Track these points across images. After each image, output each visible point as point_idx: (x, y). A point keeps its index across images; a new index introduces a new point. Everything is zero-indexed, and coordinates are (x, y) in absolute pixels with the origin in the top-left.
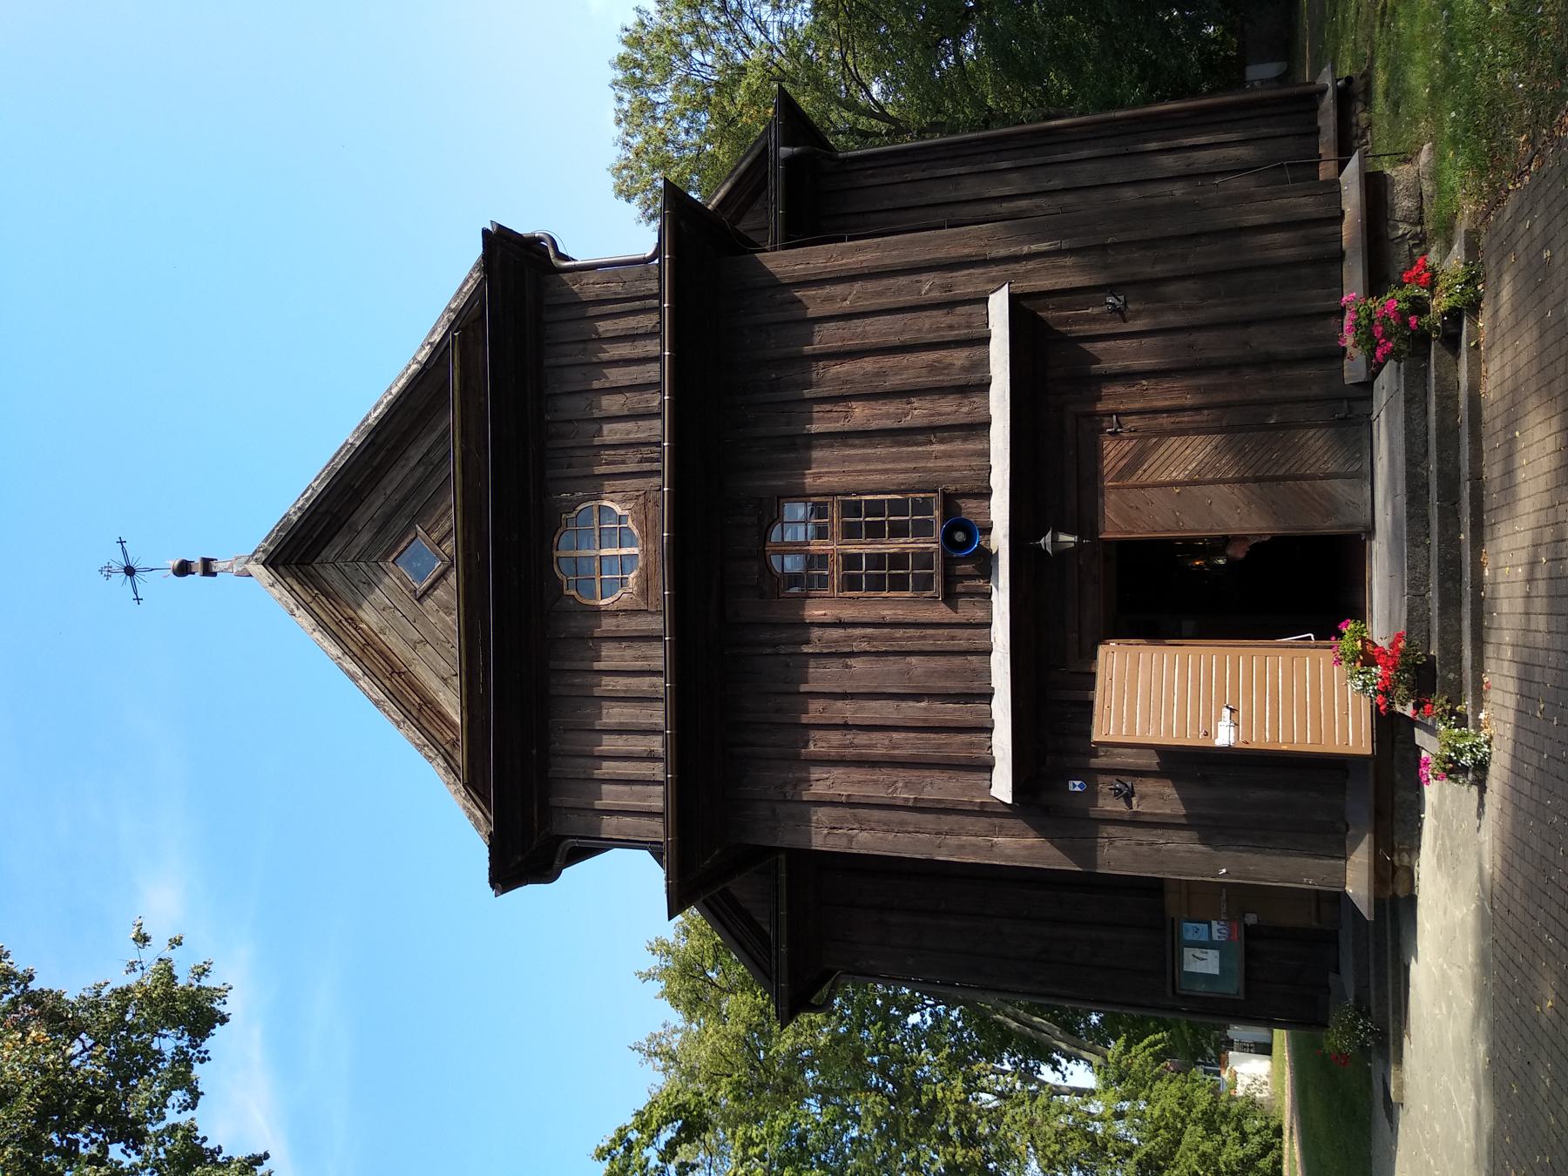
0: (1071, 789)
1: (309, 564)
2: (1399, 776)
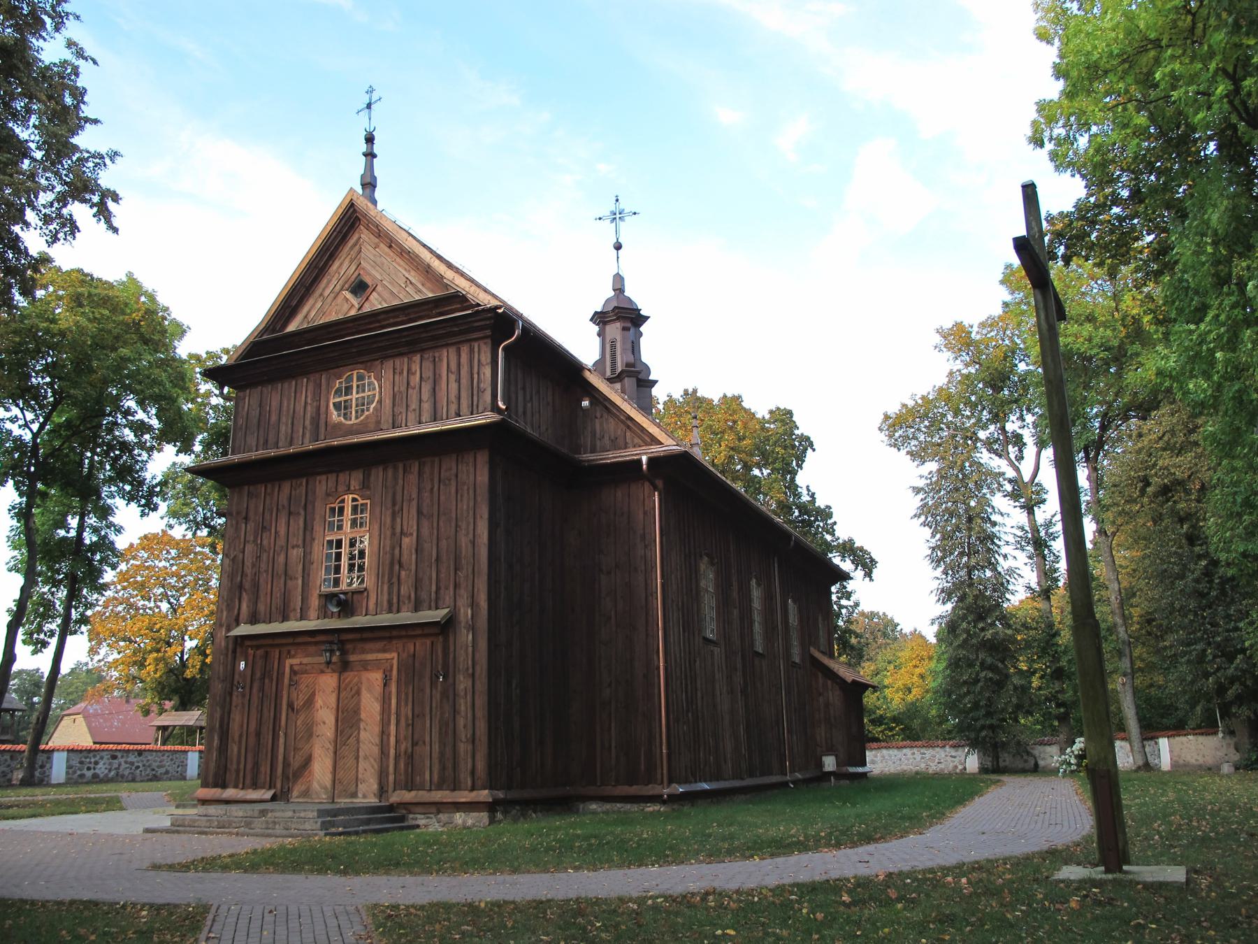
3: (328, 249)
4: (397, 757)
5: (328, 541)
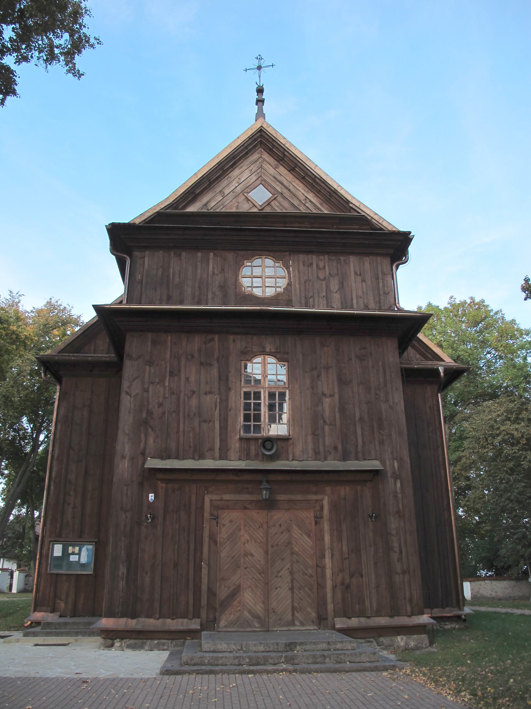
0: (150, 495)
1: (261, 146)
2: (156, 642)
3: (234, 158)
4: (334, 587)
5: (245, 393)
